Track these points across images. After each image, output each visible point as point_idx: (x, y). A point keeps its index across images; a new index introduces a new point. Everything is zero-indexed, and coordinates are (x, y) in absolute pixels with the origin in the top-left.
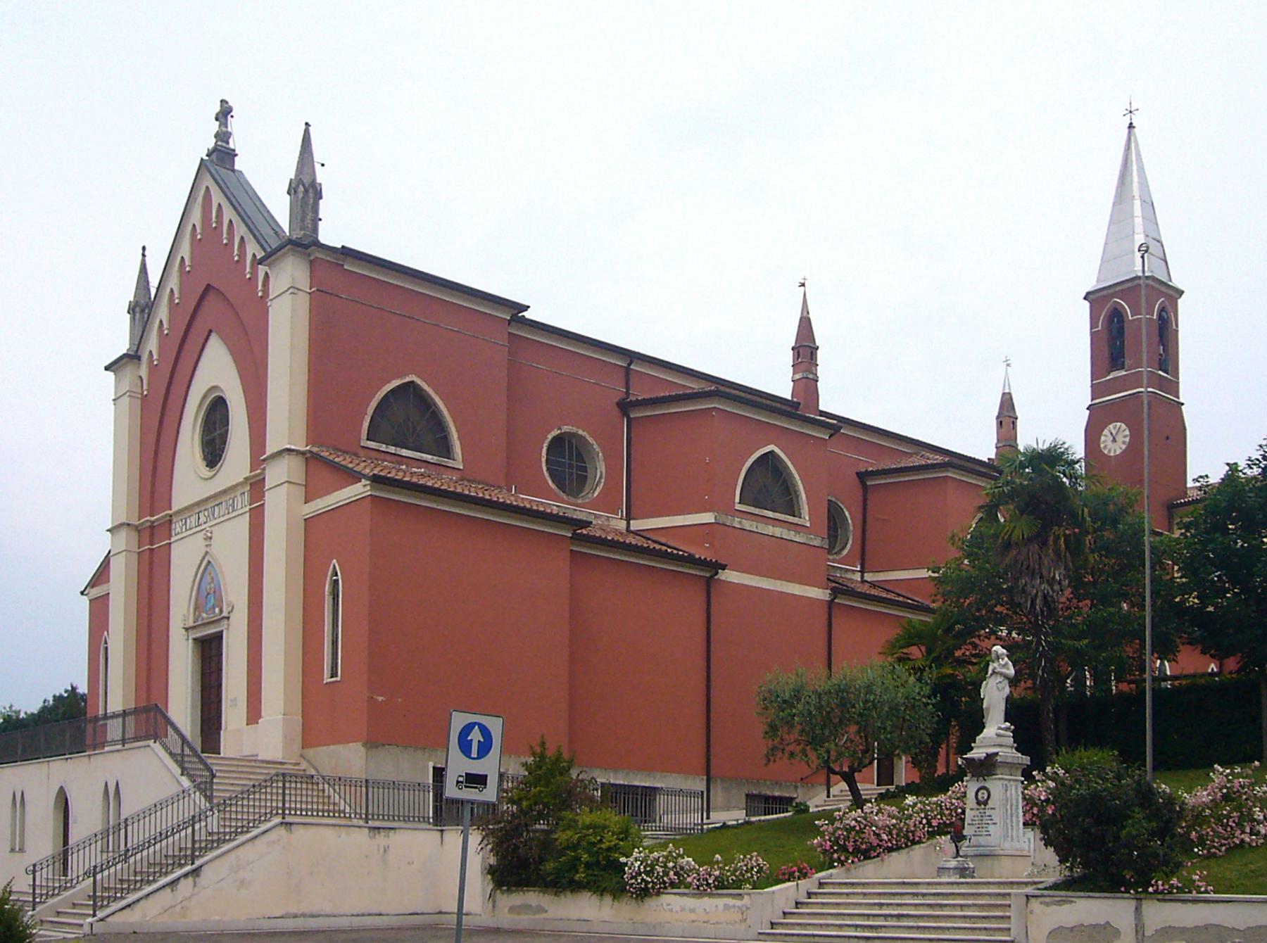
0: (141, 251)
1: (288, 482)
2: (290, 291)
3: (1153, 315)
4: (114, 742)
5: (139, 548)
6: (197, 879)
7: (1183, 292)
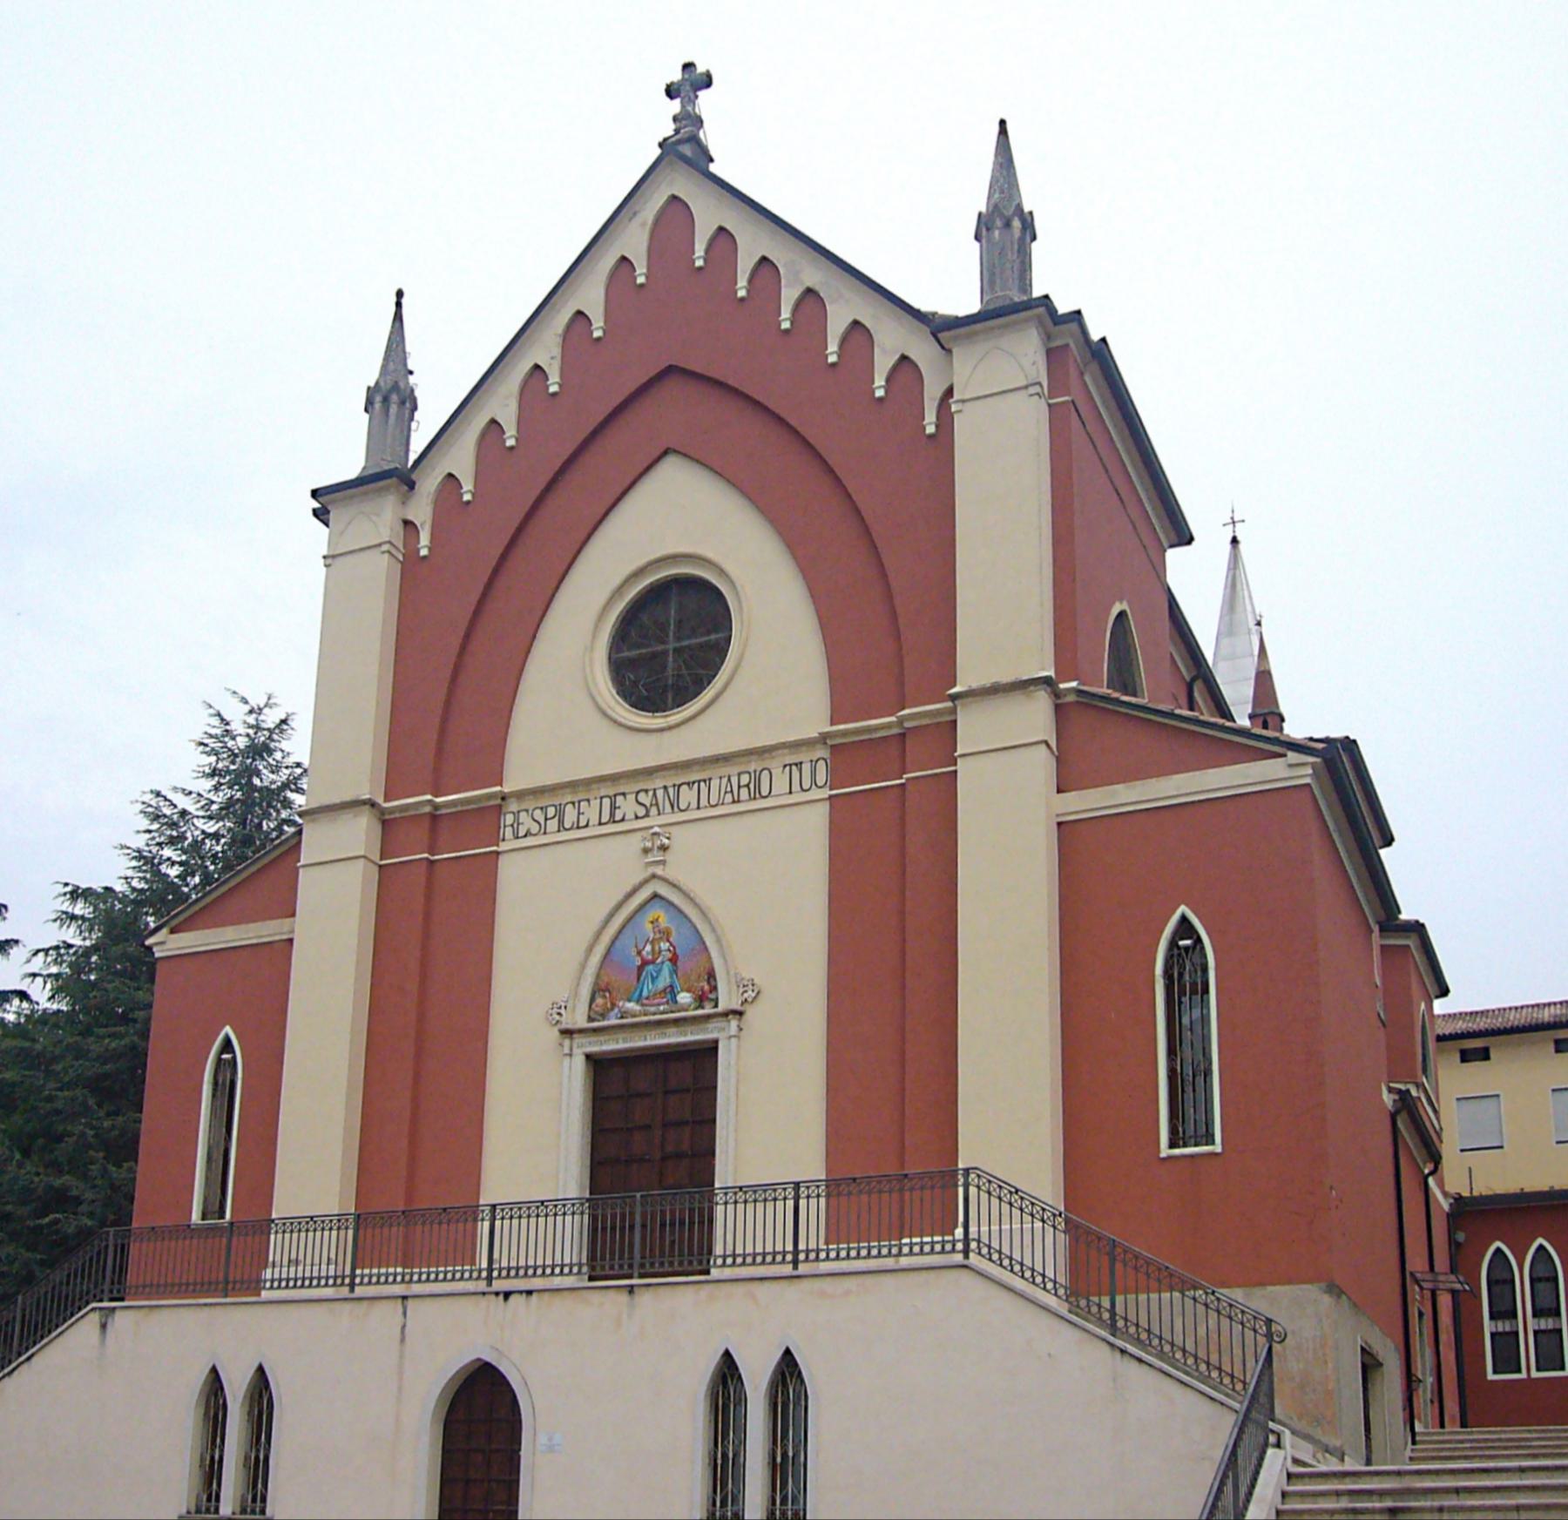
0: (394, 299)
1: (364, 857)
2: (1032, 390)
5: (381, 859)
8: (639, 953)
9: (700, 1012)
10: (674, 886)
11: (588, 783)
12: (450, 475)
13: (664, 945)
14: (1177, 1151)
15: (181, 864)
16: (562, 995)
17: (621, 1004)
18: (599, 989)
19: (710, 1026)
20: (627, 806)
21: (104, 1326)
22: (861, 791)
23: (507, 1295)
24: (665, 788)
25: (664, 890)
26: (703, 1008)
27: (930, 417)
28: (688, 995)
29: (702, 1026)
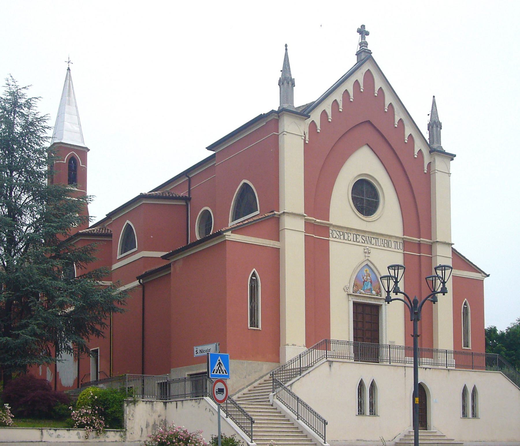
3: (64, 161)
4: (442, 365)
6: (216, 434)
7: (89, 150)
8: (363, 278)
9: (377, 297)
10: (363, 262)
11: (351, 229)
12: (313, 121)
13: (369, 278)
14: (465, 348)
15: (14, 176)
16: (347, 284)
17: (360, 290)
18: (355, 285)
19: (381, 301)
20: (360, 239)
21: (330, 366)
22: (411, 254)
23: (426, 369)
24: (368, 237)
25: (370, 264)
26: (378, 296)
27: (426, 168)
28: (374, 292)
29: (379, 301)
